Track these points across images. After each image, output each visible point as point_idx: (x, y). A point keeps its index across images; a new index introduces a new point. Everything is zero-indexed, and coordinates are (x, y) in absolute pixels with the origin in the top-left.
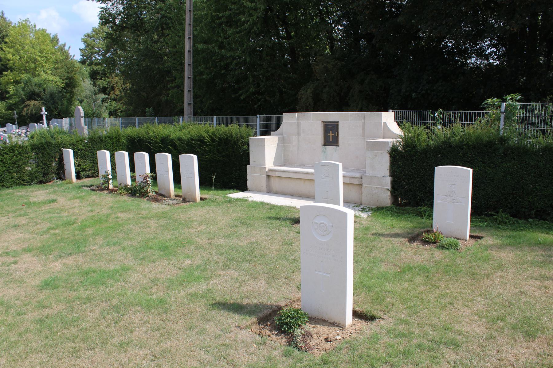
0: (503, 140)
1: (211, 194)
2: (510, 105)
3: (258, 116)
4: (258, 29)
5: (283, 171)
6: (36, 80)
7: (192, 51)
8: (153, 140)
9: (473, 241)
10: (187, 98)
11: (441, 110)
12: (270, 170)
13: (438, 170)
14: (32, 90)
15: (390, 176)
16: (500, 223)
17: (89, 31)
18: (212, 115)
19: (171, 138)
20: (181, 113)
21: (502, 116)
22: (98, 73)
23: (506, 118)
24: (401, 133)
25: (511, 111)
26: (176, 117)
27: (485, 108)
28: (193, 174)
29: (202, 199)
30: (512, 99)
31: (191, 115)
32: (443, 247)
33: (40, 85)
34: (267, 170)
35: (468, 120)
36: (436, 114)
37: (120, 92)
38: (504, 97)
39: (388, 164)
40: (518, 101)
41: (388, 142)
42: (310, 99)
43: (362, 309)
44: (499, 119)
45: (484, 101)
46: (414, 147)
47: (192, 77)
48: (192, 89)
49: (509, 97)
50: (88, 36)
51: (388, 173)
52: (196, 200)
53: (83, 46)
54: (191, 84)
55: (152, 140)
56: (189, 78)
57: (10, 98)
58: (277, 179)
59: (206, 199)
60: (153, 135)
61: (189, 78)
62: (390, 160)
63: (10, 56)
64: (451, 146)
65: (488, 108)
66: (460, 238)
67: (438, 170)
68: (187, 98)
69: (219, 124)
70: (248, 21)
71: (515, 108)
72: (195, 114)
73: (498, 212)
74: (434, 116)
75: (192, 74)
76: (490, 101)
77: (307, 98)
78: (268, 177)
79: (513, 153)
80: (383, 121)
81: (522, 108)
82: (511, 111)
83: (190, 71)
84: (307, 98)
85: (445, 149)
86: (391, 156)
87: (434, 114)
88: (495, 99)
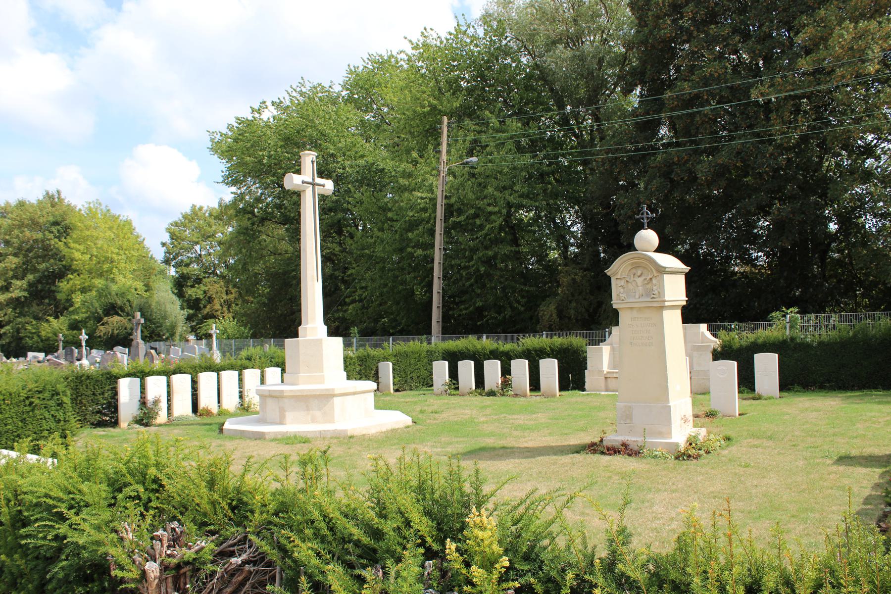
0: (792, 339)
1: (563, 393)
2: (793, 317)
5: (613, 373)
6: (114, 288)
12: (608, 373)
13: (756, 356)
14: (112, 301)
17: (177, 217)
21: (788, 326)
22: (189, 278)
23: (791, 327)
26: (425, 336)
27: (770, 321)
30: (791, 312)
32: (766, 399)
33: (123, 295)
34: (605, 372)
36: (733, 326)
37: (221, 306)
40: (797, 313)
43: (741, 412)
44: (785, 328)
45: (769, 315)
46: (731, 347)
50: (176, 224)
53: (166, 238)
57: (75, 312)
58: (614, 380)
63: (77, 255)
64: (757, 345)
66: (770, 395)
67: (756, 356)
71: (797, 319)
76: (774, 314)
77: (551, 315)
78: (606, 378)
80: (701, 331)
81: (802, 318)
84: (551, 315)
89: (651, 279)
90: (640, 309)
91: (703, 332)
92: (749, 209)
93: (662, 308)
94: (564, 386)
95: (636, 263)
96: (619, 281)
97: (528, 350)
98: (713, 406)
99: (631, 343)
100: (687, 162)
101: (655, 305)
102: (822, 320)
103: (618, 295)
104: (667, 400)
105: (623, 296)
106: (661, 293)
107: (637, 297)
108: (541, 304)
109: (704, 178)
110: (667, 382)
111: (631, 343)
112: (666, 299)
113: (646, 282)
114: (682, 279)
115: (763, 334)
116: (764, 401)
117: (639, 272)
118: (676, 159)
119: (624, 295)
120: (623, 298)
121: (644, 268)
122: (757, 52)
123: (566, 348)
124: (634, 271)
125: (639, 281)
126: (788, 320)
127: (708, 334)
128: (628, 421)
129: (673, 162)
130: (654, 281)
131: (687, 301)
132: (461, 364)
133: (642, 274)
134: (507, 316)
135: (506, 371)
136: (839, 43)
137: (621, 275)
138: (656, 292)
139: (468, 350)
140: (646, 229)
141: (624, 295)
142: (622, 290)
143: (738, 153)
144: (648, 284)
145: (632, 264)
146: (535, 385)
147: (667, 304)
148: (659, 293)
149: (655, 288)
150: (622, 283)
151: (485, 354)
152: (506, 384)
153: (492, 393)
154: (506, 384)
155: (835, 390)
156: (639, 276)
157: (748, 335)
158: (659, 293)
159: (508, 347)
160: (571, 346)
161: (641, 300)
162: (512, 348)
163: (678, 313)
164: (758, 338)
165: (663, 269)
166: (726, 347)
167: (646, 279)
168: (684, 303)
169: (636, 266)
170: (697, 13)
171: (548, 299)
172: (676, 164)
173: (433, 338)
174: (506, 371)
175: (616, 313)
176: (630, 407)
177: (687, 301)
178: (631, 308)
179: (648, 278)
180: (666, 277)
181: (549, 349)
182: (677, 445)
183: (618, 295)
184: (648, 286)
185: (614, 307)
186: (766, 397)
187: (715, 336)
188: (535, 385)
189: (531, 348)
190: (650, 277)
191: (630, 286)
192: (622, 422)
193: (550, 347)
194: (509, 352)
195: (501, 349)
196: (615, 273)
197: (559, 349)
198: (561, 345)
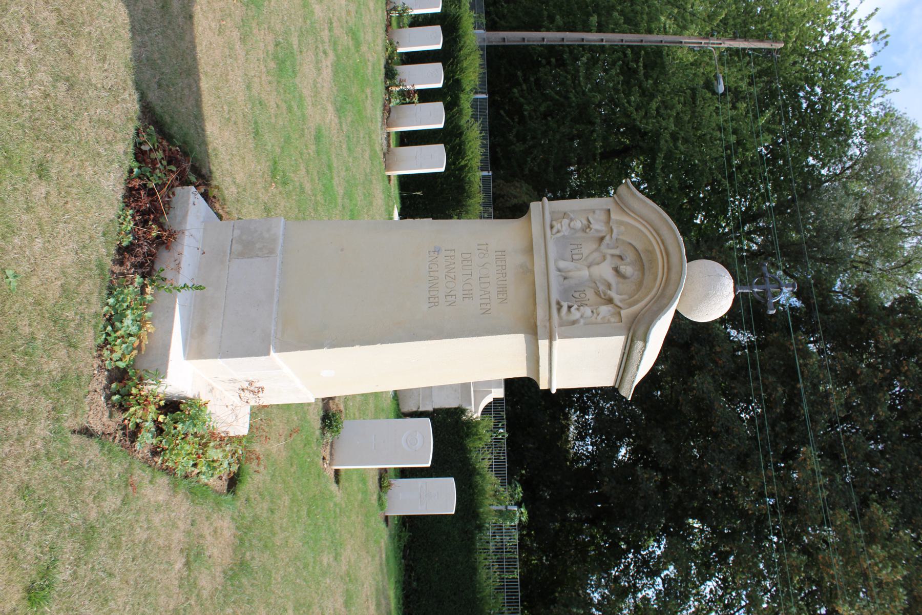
0: (480, 528)
1: (394, 182)
2: (515, 514)
3: (491, 173)
4: (618, 118)
7: (582, 43)
8: (456, 67)
9: (333, 473)
10: (514, 37)
11: (507, 435)
15: (434, 409)
16: (400, 537)
18: (490, 93)
19: (461, 96)
20: (492, 26)
21: (502, 508)
24: (398, 51)
25: (508, 516)
26: (484, 21)
27: (510, 483)
28: (421, 168)
29: (389, 176)
30: (522, 513)
31: (489, 42)
32: (380, 498)
35: (496, 468)
36: (501, 431)
38: (523, 504)
39: (447, 406)
40: (520, 520)
41: (470, 404)
42: (515, 201)
46: (467, 435)
47: (545, 43)
48: (526, 43)
49: (523, 510)
51: (437, 406)
52: (388, 171)
54: (533, 41)
55: (457, 65)
56: (543, 39)
59: (389, 183)
60: (465, 65)
61: (543, 39)
62: (451, 409)
64: (471, 475)
65: (512, 488)
68: (514, 37)
69: (484, 178)
70: (630, 105)
71: (512, 520)
72: (489, 48)
73: (409, 531)
74: (499, 428)
75: (549, 43)
76: (519, 489)
77: (515, 197)
79: (468, 540)
82: (508, 516)
83: (555, 41)
84: (515, 197)
85: (468, 470)
86: (456, 409)
87: (503, 428)
88: (521, 495)
89: (610, 301)
90: (528, 271)
91: (490, 392)
92: (653, 441)
93: (532, 332)
94: (407, 183)
95: (653, 261)
96: (602, 217)
97: (461, 134)
98: (349, 427)
99: (437, 251)
100: (715, 363)
101: (541, 313)
102: (509, 555)
103: (565, 215)
104: (285, 347)
105: (563, 226)
106: (573, 329)
107: (562, 264)
108: (529, 184)
109: (695, 385)
110: (332, 346)
111: (437, 251)
112: (558, 343)
113: (602, 288)
114: (606, 379)
115: (490, 482)
116: (375, 497)
117: (627, 269)
118: (718, 349)
119: (565, 231)
120: (557, 226)
121: (640, 284)
122: (854, 454)
123: (464, 189)
124: (630, 256)
125: (605, 271)
126: (510, 508)
127: (488, 399)
128: (237, 247)
129: (714, 346)
130: (605, 310)
131: (549, 391)
132: (437, 29)
133: (623, 276)
134: (513, 147)
135: (426, 96)
136: (876, 564)
137: (621, 223)
138: (575, 314)
139: (460, 50)
140: (735, 291)
141: (565, 231)
142: (578, 224)
143: (728, 431)
144: (597, 293)
145: (651, 252)
146: (408, 139)
147: (543, 344)
148: (574, 322)
149: (587, 311)
150: (598, 226)
151: (454, 72)
152: (406, 96)
153: (390, 74)
154: (406, 96)
155: (403, 589)
156: (616, 270)
157: (486, 461)
158: (574, 322)
159: (466, 104)
160: (469, 197)
161: (553, 273)
162: (464, 112)
163: (520, 371)
164: (483, 476)
165: (640, 332)
166: (468, 428)
167: (609, 286)
168: (543, 386)
169: (643, 262)
170: (906, 376)
171: (536, 193)
172: (711, 350)
173: (482, 31)
174: (426, 96)
175: (518, 211)
176: (272, 252)
177: (549, 391)
178: (530, 250)
179: (613, 294)
180: (617, 343)
181: (463, 163)
182: (160, 373)
183: (565, 215)
184: (590, 294)
185: (534, 206)
186: (385, 497)
187: (486, 410)
188: (408, 139)
189: (463, 138)
190: (617, 298)
191: (588, 248)
192: (237, 232)
193: (466, 165)
194: (458, 106)
195: (463, 97)
196: (623, 206)
197: (463, 179)
198: (470, 182)
